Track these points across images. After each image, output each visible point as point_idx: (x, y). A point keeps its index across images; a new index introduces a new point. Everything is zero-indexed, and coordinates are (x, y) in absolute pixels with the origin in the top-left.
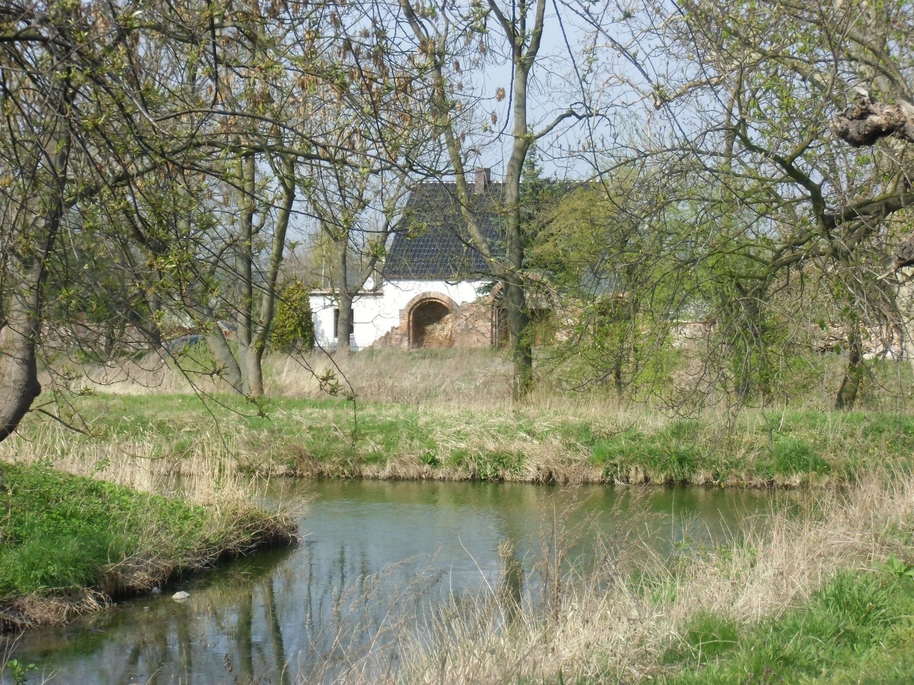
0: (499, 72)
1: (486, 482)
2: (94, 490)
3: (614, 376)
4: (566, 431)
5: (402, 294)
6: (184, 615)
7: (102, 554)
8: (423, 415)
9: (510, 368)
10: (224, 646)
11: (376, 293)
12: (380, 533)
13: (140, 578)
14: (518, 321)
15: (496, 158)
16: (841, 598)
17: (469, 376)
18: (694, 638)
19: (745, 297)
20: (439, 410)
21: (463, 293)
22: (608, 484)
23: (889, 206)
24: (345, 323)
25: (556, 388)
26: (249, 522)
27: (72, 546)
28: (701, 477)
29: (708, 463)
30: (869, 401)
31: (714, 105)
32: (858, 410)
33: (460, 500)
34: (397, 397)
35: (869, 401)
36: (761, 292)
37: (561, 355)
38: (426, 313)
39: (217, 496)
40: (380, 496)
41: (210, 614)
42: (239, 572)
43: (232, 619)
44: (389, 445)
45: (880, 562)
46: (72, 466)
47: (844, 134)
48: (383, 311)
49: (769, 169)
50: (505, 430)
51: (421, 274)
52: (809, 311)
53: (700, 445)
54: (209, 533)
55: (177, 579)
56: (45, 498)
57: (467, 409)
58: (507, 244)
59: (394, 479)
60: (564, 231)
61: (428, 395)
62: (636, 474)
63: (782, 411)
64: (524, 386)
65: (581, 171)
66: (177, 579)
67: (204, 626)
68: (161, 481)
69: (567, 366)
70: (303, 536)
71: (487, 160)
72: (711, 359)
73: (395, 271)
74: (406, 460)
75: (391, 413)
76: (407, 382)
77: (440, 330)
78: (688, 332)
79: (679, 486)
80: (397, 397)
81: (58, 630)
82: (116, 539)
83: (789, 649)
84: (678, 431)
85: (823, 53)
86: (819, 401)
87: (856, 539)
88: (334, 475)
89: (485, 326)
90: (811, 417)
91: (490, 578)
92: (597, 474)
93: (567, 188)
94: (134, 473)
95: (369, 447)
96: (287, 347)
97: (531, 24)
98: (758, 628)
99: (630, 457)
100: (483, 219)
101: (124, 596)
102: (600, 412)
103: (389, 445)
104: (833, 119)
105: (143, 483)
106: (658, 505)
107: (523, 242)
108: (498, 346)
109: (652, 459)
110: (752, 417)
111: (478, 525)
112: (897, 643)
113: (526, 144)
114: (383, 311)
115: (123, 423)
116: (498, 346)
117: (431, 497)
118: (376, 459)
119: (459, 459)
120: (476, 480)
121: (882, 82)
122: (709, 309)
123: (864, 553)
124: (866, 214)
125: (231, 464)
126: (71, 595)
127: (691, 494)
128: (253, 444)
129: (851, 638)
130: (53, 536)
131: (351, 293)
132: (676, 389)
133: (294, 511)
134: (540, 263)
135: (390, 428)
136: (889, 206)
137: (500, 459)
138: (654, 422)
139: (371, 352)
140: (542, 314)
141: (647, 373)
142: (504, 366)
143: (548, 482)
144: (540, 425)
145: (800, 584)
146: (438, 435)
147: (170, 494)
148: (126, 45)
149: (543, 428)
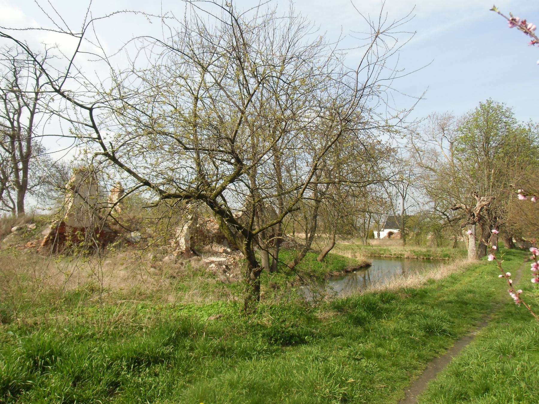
0: (400, 200)
1: (399, 258)
2: (343, 257)
3: (418, 243)
4: (411, 251)
5: (387, 231)
6: (356, 274)
7: (344, 266)
8: (390, 248)
9: (402, 242)
10: (362, 279)
11: (383, 231)
12: (384, 265)
13: (349, 269)
14: (404, 236)
15: (400, 212)
16: (452, 277)
17: (397, 243)
18: (428, 282)
19: (438, 231)
20: (392, 247)
21: (395, 231)
22: (417, 259)
23: (460, 219)
24: (379, 235)
25: (410, 245)
26: (364, 262)
27: (340, 265)
28: (431, 258)
29: (433, 256)
30: (458, 247)
31: (432, 204)
32: (456, 249)
33: (395, 260)
34: (386, 245)
35: (458, 247)
36: (440, 231)
37: (410, 240)
38: (390, 234)
39: (360, 259)
40: (384, 259)
41: (359, 275)
42: (363, 269)
43: (363, 275)
44: (385, 252)
45: (458, 272)
46: (340, 254)
47: (452, 209)
48: (384, 233)
49: (441, 214)
50: (402, 250)
51: (391, 228)
52: (448, 234)
53: (431, 253)
54: (359, 264)
55: (354, 270)
56: (336, 258)
57: (396, 248)
58: (403, 224)
59: (385, 257)
60: (410, 223)
61: (390, 245)
62: (422, 257)
63: (444, 249)
64: (405, 244)
65: (412, 214)
66: (354, 270)
67: (359, 276)
68: (352, 257)
69: (411, 242)
70: (372, 264)
71: (399, 212)
72: (432, 241)
73: (386, 227)
74: (387, 254)
75: (385, 248)
76: (387, 243)
77: (392, 236)
78: (429, 237)
79: (428, 259)
80: (386, 245)
81: (338, 276)
82: (346, 264)
83: (443, 284)
84: (428, 251)
85: (449, 197)
86: (450, 248)
87: (455, 268)
88: (376, 256)
89: (399, 236)
90: (449, 249)
91: (399, 271)
92: (416, 257)
93: (411, 216)
94: (349, 255)
95: (382, 252)
96: (370, 238)
97: (405, 194)
98: (439, 280)
99: (421, 255)
100: (398, 221)
101: (347, 272)
102: (416, 248)
103: (385, 252)
104: (450, 206)
105: (350, 257)
106: (424, 262)
107: (404, 224)
108: (401, 238)
109: (425, 255)
110: (439, 249)
111: (398, 264)
112: (461, 284)
113: (404, 210)
114: (384, 233)
115: (346, 248)
116: (401, 238)
117: (391, 260)
118: (383, 254)
119: (395, 254)
120: (398, 257)
121: (459, 201)
122: (432, 233)
123: (456, 270)
124: (456, 220)
125: (362, 254)
126: (339, 271)
127: (429, 260)
128: (365, 252)
129: (453, 283)
130: (337, 263)
131: (379, 231)
132: (428, 244)
133: (371, 261)
134: (407, 227)
135: (385, 250)
136: (460, 219)
137: (401, 255)
138: (424, 250)
139: (382, 239)
140: (407, 234)
141: (423, 242)
142: (402, 241)
143: (408, 258)
144: (407, 250)
145: (445, 274)
146: (392, 251)
147: (354, 258)
148: (202, 387)
149: (407, 251)
